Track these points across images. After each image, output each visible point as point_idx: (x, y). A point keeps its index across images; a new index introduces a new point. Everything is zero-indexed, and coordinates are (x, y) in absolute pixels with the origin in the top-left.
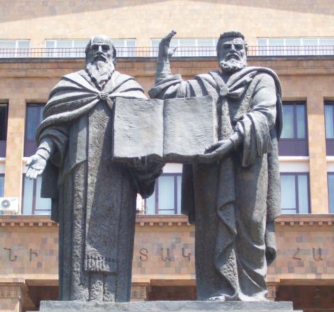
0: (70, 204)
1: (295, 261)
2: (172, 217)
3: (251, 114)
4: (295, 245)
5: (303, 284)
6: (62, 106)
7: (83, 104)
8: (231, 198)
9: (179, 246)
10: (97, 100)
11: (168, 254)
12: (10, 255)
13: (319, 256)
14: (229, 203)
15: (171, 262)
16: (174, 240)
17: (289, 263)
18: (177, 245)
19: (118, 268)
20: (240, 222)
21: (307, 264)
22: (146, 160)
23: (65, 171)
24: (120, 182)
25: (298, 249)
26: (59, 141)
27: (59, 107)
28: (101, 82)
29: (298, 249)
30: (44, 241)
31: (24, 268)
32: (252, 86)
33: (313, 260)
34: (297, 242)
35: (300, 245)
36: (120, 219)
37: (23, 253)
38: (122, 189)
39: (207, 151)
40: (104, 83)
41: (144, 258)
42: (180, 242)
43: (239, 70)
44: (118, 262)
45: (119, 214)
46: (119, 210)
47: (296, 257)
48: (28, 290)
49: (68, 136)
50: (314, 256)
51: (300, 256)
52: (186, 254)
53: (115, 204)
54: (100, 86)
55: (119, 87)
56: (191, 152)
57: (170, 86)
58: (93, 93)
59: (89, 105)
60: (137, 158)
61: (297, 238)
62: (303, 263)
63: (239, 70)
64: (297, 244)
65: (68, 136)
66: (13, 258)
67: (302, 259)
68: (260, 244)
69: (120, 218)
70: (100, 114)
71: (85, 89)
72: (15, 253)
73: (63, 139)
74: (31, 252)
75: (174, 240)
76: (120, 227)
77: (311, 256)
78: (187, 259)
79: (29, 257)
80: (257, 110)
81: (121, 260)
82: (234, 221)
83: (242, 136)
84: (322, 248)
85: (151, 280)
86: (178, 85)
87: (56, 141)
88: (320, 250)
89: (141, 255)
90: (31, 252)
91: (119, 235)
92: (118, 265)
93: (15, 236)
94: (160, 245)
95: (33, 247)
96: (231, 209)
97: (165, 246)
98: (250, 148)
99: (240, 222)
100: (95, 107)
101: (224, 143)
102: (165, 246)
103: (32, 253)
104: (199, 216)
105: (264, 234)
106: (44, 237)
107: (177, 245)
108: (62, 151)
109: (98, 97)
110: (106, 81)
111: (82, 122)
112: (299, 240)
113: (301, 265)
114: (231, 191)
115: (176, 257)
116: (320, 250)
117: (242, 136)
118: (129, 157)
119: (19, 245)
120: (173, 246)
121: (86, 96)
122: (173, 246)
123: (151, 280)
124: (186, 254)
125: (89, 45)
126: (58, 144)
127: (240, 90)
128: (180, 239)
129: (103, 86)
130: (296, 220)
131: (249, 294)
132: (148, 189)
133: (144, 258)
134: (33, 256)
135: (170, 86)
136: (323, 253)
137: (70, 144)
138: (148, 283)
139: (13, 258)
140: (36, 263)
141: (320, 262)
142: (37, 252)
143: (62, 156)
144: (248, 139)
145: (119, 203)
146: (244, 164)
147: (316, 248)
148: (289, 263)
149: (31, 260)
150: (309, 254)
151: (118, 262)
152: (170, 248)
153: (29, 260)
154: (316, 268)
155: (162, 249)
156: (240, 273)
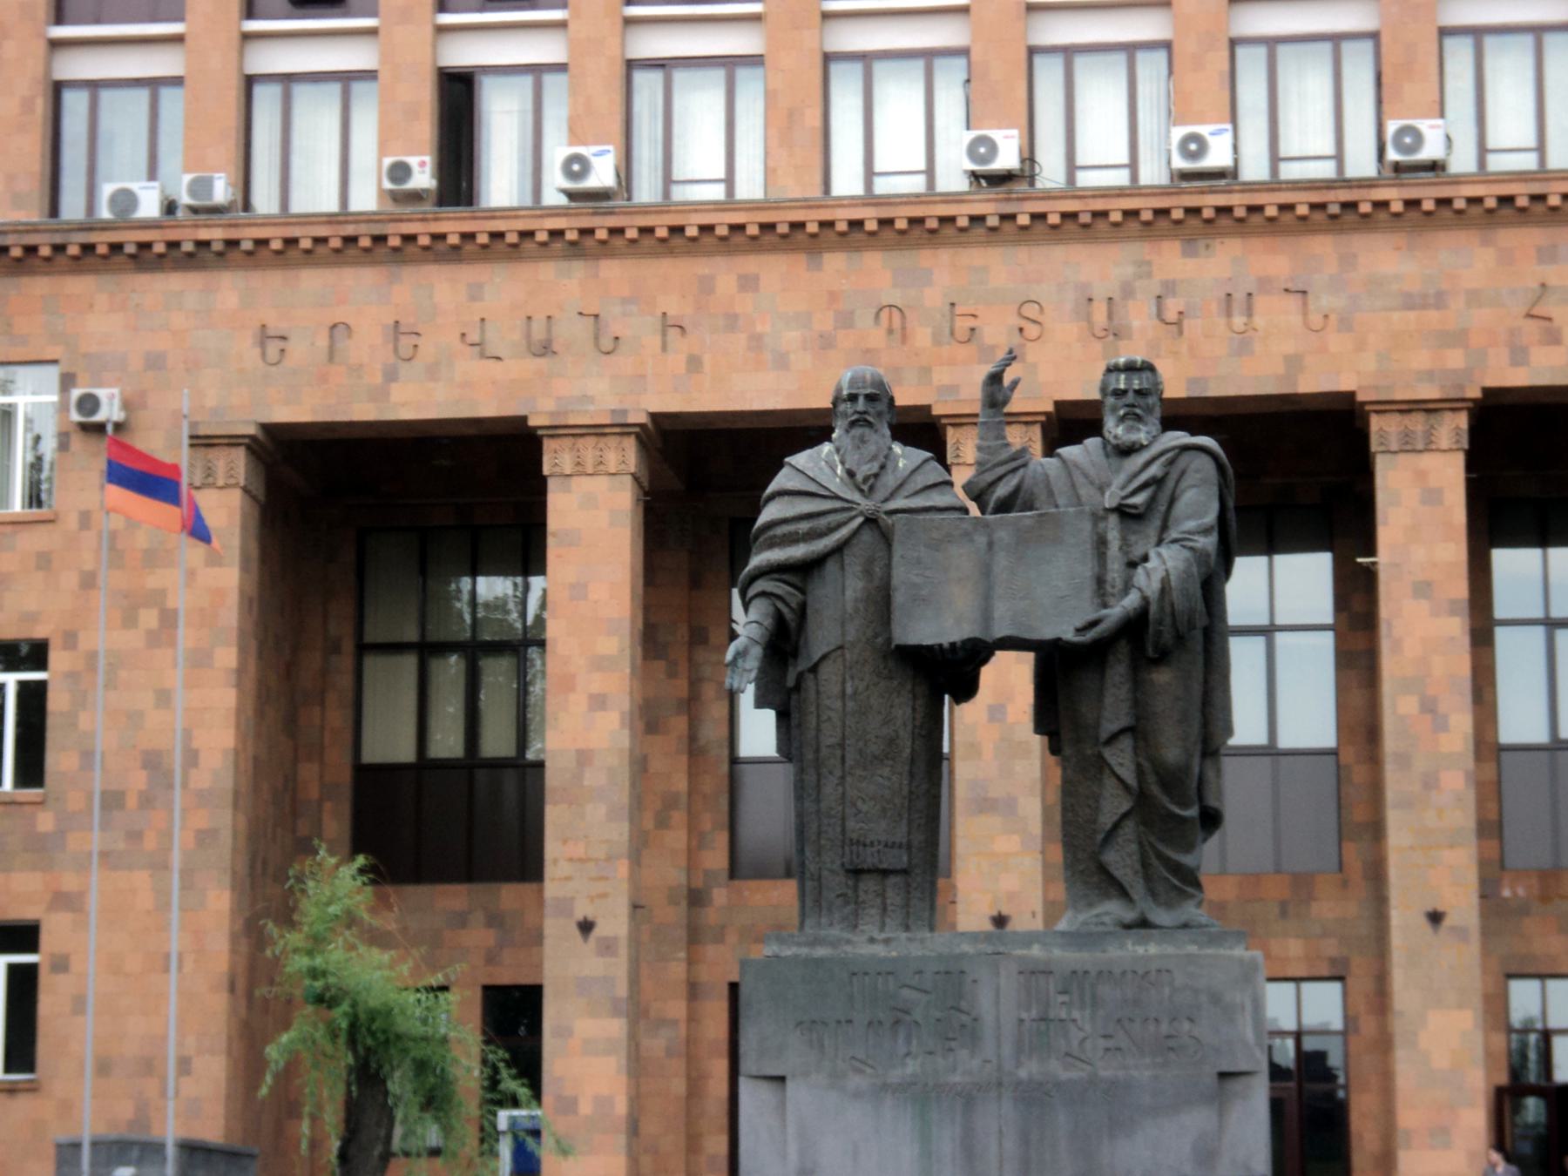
0: (812, 733)
1: (1532, 325)
2: (1120, 192)
3: (1104, 736)
6: (790, 533)
7: (831, 530)
8: (1124, 721)
9: (1146, 291)
10: (860, 520)
11: (1110, 316)
12: (597, 338)
14: (1122, 731)
16: (1129, 270)
20: (1146, 765)
24: (909, 687)
25: (1543, 285)
26: (787, 605)
28: (866, 479)
29: (1543, 285)
30: (706, 286)
31: (643, 377)
32: (1170, 484)
34: (1541, 261)
36: (913, 761)
37: (639, 329)
39: (1079, 631)
40: (872, 481)
41: (1032, 331)
42: (1149, 275)
43: (1142, 447)
45: (908, 751)
46: (909, 743)
47: (1534, 312)
51: (1548, 308)
52: (1171, 315)
53: (901, 733)
54: (865, 488)
55: (901, 485)
57: (1000, 478)
58: (849, 506)
59: (844, 532)
61: (1539, 250)
63: (1142, 447)
66: (607, 343)
68: (1185, 806)
72: (616, 328)
73: (794, 598)
74: (667, 324)
76: (912, 775)
78: (1174, 328)
79: (658, 340)
80: (1175, 541)
81: (915, 843)
82: (1133, 767)
83: (1145, 599)
86: (1021, 471)
87: (780, 605)
89: (1023, 323)
90: (667, 324)
91: (911, 792)
93: (612, 270)
95: (673, 306)
96: (1126, 743)
97: (1100, 291)
98: (1160, 622)
99: (1146, 765)
101: (1106, 616)
102: (1100, 291)
104: (1067, 751)
107: (1138, 284)
108: (793, 625)
109: (861, 513)
110: (876, 476)
111: (831, 567)
112: (1547, 255)
114: (1125, 708)
115: (1136, 324)
117: (1145, 599)
119: (625, 301)
120: (1128, 291)
122: (1128, 291)
123: (1057, 404)
124: (1171, 315)
125: (839, 390)
126: (785, 610)
127: (1139, 499)
128: (1149, 263)
129: (871, 488)
130: (1537, 188)
132: (966, 689)
133: (1032, 331)
134: (673, 333)
135: (1000, 478)
137: (809, 611)
138: (1046, 414)
139: (607, 343)
144: (1153, 609)
145: (910, 727)
146: (1150, 652)
149: (664, 347)
151: (909, 847)
155: (1090, 300)
156: (1145, 865)
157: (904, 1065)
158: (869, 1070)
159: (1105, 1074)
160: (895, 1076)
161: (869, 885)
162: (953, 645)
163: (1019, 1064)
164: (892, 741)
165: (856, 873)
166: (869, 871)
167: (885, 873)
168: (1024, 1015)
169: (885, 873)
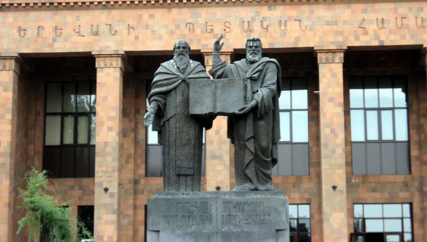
3: (246, 139)
4: (360, 16)
5: (368, 50)
7: (173, 83)
9: (258, 19)
11: (249, 26)
12: (110, 31)
13: (381, 25)
15: (252, 33)
16: (254, 14)
17: (355, 32)
18: (256, 18)
19: (193, 172)
21: (371, 33)
22: (215, 60)
23: (165, 119)
26: (161, 103)
27: (160, 84)
28: (182, 69)
29: (363, 19)
31: (123, 41)
33: (376, 28)
34: (363, 13)
35: (366, 16)
37: (122, 28)
38: (195, 129)
39: (239, 110)
41: (228, 30)
42: (259, 15)
43: (257, 61)
44: (193, 169)
46: (193, 141)
48: (127, 60)
49: (165, 100)
50: (377, 25)
53: (192, 138)
54: (182, 72)
56: (231, 111)
57: (219, 69)
58: (178, 77)
59: (176, 84)
60: (202, 114)
61: (362, 10)
62: (368, 31)
63: (257, 61)
64: (362, 15)
65: (165, 100)
66: (113, 32)
67: (367, 29)
68: (268, 157)
69: (194, 145)
70: (183, 85)
71: (175, 74)
72: (116, 28)
73: (163, 101)
75: (254, 14)
77: (375, 25)
79: (127, 31)
83: (257, 102)
84: (385, 18)
85: (234, 49)
86: (224, 68)
87: (159, 103)
88: (383, 20)
89: (225, 28)
90: (130, 28)
91: (194, 154)
92: (194, 171)
94: (242, 18)
95: (131, 22)
96: (252, 140)
97: (246, 20)
98: (261, 108)
100: (181, 82)
102: (246, 20)
103: (130, 28)
105: (271, 148)
106: (140, 13)
107: (256, 18)
108: (162, 108)
110: (185, 68)
111: (173, 93)
112: (365, 11)
113: (366, 33)
114: (252, 131)
115: (255, 28)
116: (383, 20)
117: (257, 102)
118: (198, 113)
119: (118, 21)
120: (253, 19)
121: (174, 78)
122: (253, 19)
124: (265, 26)
127: (256, 75)
128: (259, 12)
129: (184, 72)
131: (263, 184)
132: (209, 126)
133: (228, 30)
134: (131, 30)
135: (219, 69)
136: (386, 22)
139: (113, 32)
140: (134, 36)
141: (383, 30)
142: (135, 27)
143: (163, 111)
144: (259, 105)
146: (259, 116)
147: (380, 18)
148: (355, 32)
149: (129, 34)
150: (373, 23)
151: (193, 169)
152: (250, 21)
153: (127, 34)
154: (379, 36)
156: (257, 174)
157: (191, 227)
158: (182, 229)
159: (246, 230)
160: (189, 230)
161: (182, 179)
162: (205, 114)
163: (222, 227)
164: (189, 140)
165: (179, 175)
166: (182, 175)
167: (187, 176)
168: (224, 214)
169: (187, 176)
